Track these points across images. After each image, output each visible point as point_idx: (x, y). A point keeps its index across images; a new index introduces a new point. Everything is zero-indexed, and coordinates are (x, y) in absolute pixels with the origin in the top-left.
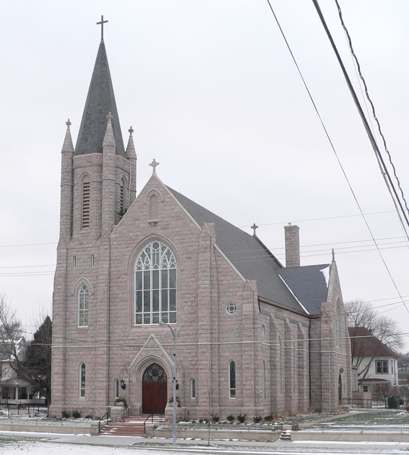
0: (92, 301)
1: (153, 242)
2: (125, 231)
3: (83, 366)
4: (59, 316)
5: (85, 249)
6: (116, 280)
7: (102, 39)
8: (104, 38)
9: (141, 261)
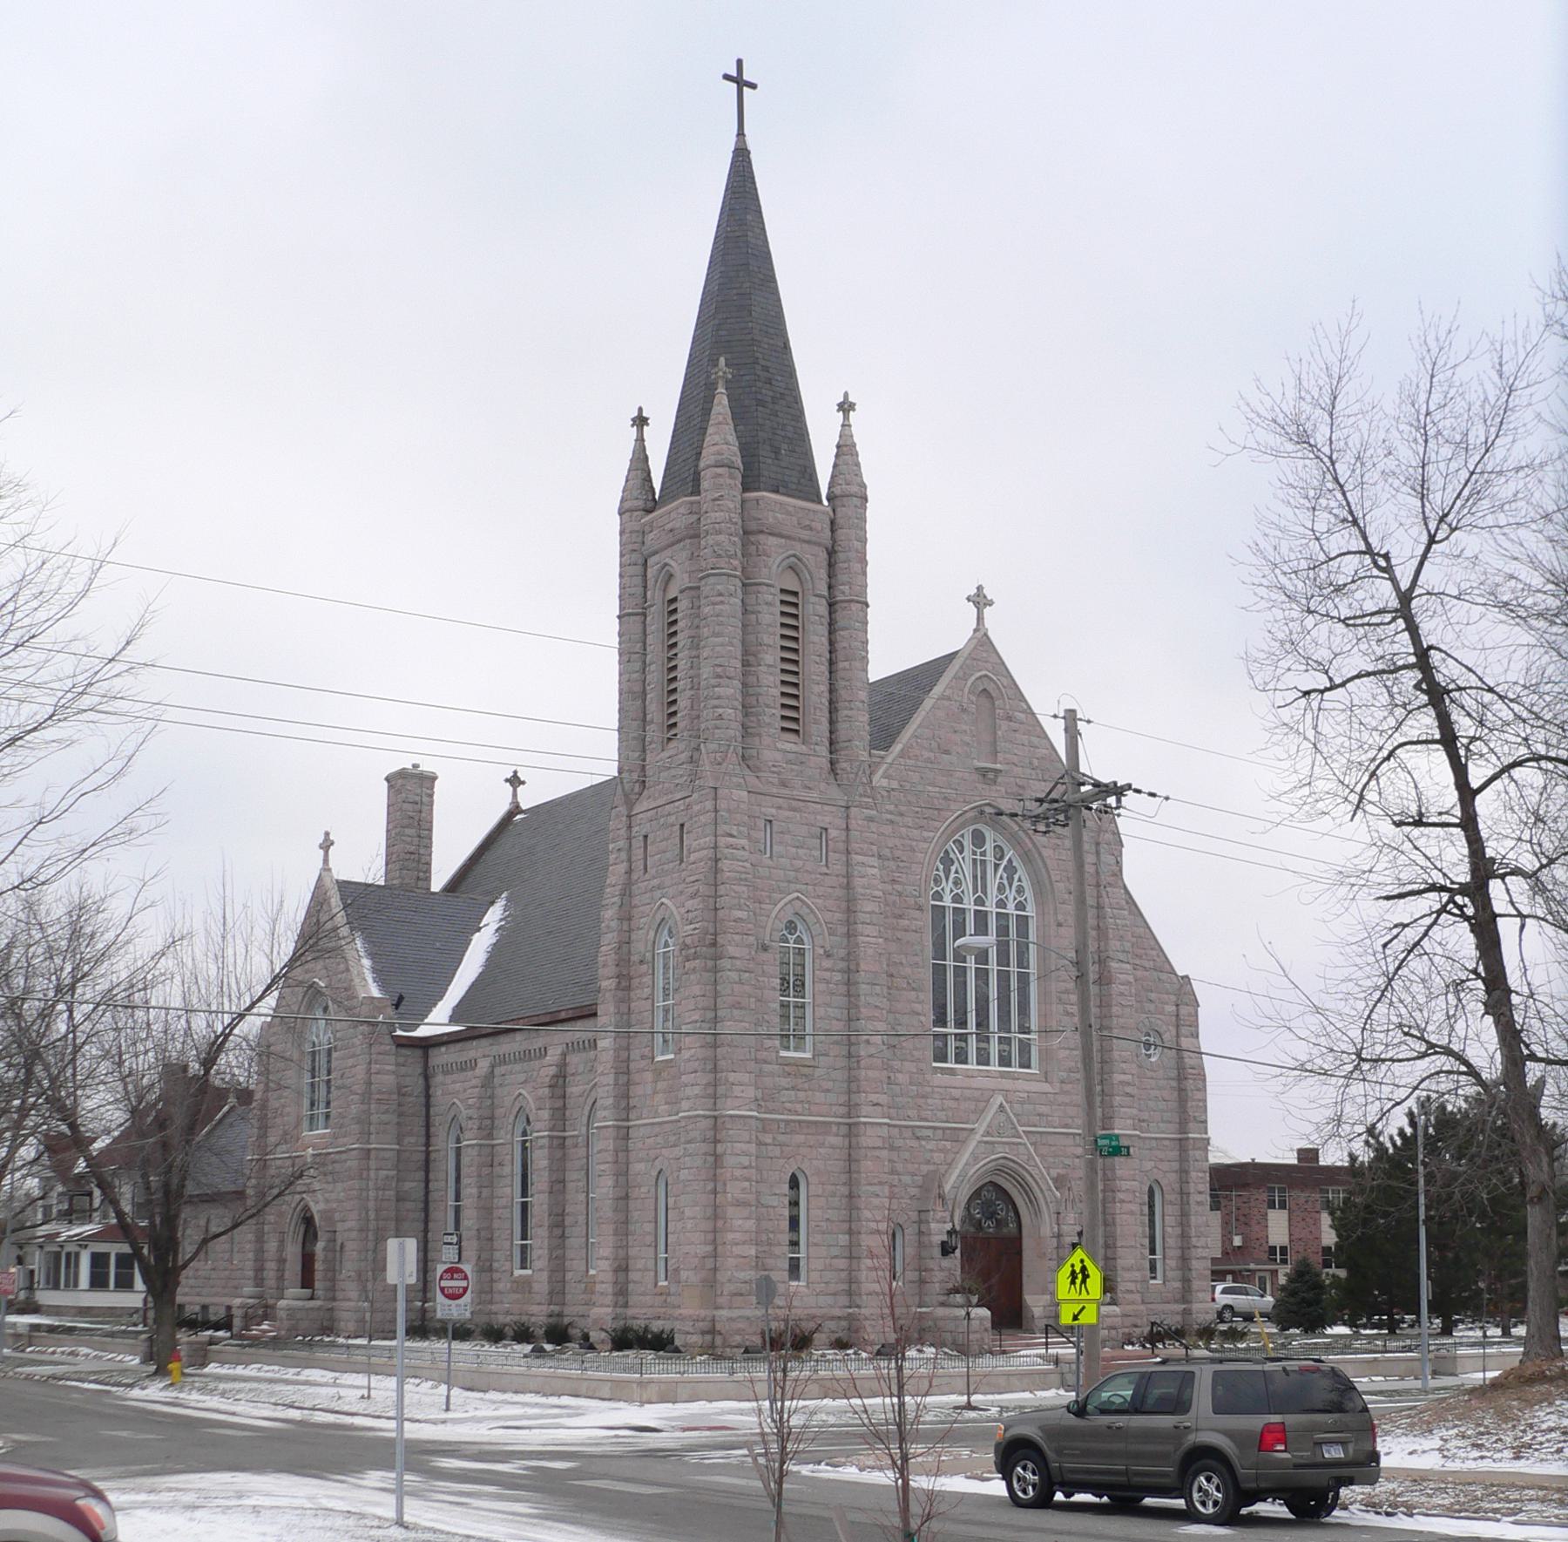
0: (827, 975)
1: (972, 828)
2: (915, 777)
3: (794, 1183)
4: (743, 1012)
5: (801, 804)
6: (894, 921)
7: (741, 134)
8: (746, 132)
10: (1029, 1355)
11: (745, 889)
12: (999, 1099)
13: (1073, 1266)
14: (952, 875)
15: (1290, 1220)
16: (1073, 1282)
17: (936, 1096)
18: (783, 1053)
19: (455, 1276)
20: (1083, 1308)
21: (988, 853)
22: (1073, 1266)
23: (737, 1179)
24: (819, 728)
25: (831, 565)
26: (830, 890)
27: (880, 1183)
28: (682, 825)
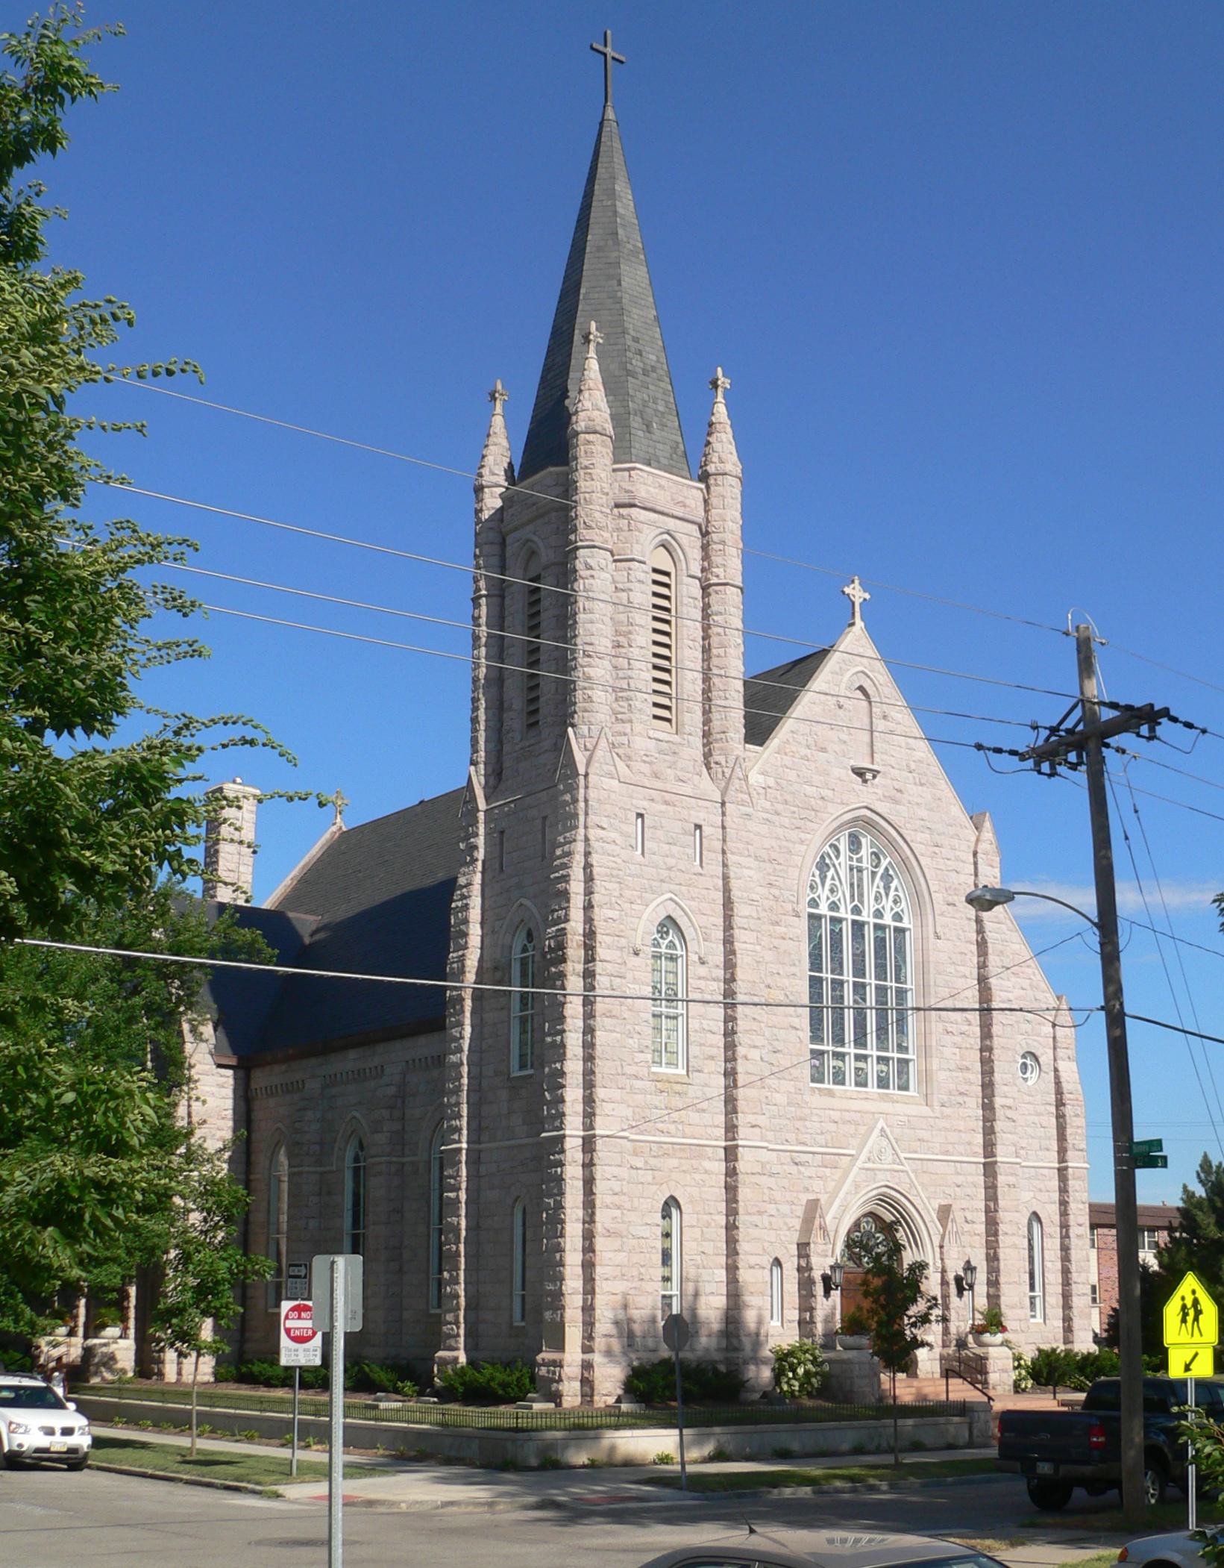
2: (792, 775)
4: (614, 1021)
6: (771, 927)
9: (818, 880)
10: (610, 1379)
11: (616, 886)
12: (881, 1124)
13: (1183, 1298)
14: (828, 882)
15: (1098, 1258)
16: (1184, 1321)
17: (815, 1118)
18: (654, 1069)
19: (303, 1315)
20: (1196, 1354)
21: (864, 860)
22: (1183, 1298)
23: (607, 1207)
24: (692, 717)
25: (705, 548)
26: (704, 892)
27: (760, 1213)
28: (545, 818)
